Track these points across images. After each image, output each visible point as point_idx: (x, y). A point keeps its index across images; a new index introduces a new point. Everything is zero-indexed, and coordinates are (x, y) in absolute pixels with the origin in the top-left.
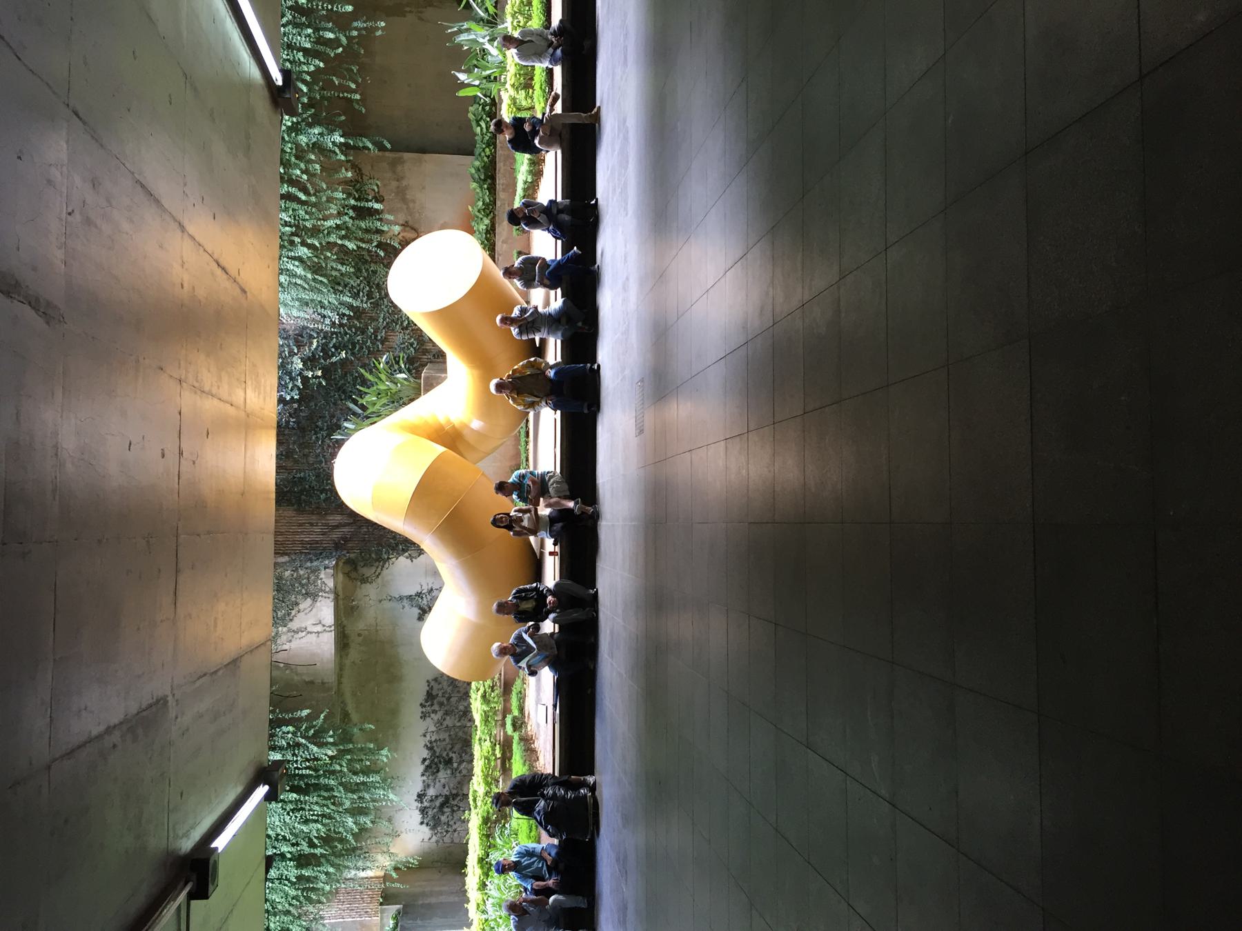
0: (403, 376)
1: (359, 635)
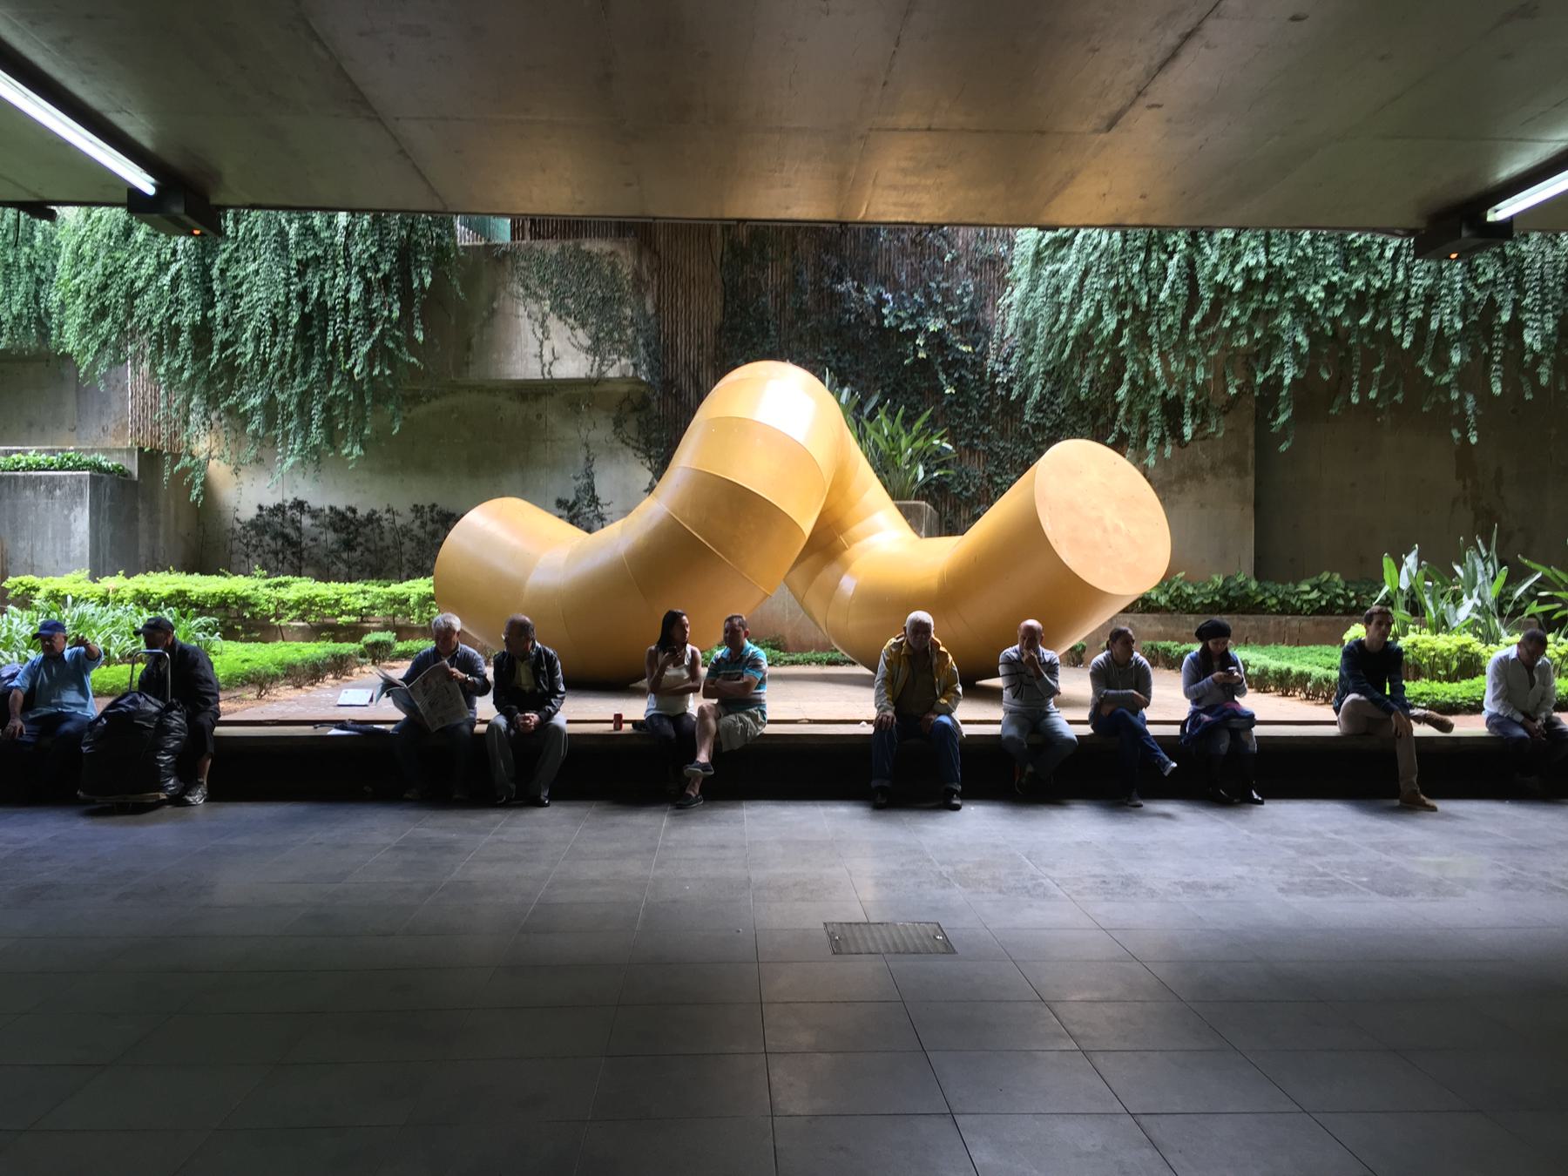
0: (921, 475)
1: (539, 416)
